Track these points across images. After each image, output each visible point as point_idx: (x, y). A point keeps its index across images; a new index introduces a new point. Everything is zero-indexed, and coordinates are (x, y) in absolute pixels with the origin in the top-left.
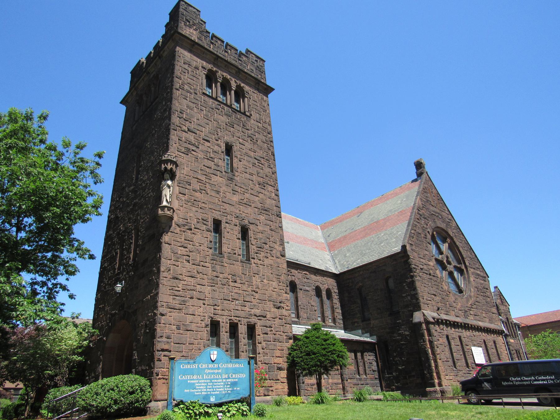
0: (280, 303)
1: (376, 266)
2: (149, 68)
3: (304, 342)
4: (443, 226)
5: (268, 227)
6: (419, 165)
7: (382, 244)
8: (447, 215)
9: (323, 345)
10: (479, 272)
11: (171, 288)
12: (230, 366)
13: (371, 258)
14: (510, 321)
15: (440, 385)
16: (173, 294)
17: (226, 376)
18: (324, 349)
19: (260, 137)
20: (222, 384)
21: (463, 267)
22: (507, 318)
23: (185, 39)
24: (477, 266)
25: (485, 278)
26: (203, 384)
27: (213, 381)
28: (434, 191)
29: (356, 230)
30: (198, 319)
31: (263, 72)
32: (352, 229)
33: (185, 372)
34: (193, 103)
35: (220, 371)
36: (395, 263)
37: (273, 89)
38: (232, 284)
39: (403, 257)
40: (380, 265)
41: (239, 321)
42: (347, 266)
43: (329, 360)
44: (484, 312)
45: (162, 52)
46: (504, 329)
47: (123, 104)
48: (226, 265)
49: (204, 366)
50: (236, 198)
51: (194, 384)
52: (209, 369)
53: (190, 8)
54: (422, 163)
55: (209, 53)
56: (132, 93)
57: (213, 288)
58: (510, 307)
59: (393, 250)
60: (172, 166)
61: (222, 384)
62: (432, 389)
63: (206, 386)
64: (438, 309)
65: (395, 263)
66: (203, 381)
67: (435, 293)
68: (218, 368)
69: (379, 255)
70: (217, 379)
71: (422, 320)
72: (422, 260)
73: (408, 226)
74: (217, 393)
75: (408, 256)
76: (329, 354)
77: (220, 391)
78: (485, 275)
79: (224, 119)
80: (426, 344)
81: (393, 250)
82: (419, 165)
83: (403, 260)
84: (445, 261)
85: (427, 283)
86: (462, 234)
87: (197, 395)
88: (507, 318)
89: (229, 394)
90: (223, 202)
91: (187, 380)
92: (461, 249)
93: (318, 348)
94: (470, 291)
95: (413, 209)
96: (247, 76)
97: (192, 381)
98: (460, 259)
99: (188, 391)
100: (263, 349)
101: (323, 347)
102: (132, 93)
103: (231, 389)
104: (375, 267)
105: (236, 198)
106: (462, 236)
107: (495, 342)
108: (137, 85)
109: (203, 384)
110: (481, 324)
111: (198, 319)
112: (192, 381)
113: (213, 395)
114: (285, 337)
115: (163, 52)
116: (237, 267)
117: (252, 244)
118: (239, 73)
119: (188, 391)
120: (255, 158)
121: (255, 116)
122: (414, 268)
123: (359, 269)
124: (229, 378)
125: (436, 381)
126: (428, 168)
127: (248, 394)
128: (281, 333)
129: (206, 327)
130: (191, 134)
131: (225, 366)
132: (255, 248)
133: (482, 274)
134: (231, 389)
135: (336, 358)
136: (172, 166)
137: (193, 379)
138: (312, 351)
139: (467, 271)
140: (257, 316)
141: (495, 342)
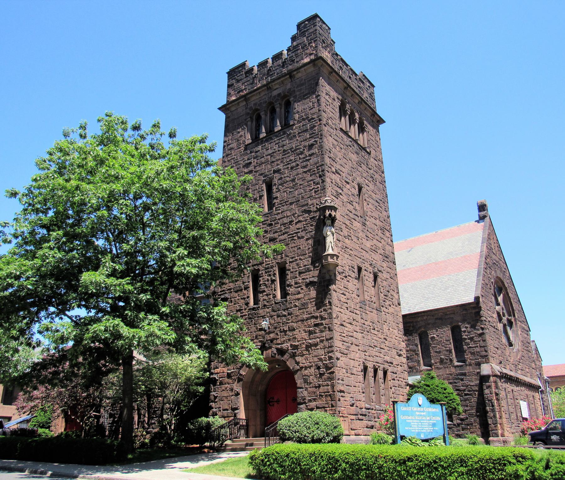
0: (400, 350)
1: (443, 313)
2: (273, 84)
3: (425, 389)
4: (501, 276)
5: (389, 274)
6: (482, 207)
7: (448, 291)
8: (502, 264)
9: (444, 393)
10: (524, 326)
11: (340, 334)
12: (430, 410)
13: (437, 303)
14: (542, 376)
15: (503, 435)
16: (342, 340)
17: (428, 418)
18: (446, 397)
19: (377, 176)
20: (427, 424)
21: (513, 320)
22: (540, 374)
23: (327, 66)
24: (523, 319)
25: (528, 331)
26: (415, 424)
27: (421, 421)
28: (495, 237)
29: (410, 269)
30: (357, 364)
31: (374, 100)
32: (404, 266)
33: (405, 413)
34: (336, 140)
35: (425, 413)
36: (464, 312)
37: (384, 122)
38: (372, 331)
39: (474, 308)
40: (448, 313)
41: (379, 367)
42: (408, 309)
43: (451, 407)
44: (527, 367)
45: (295, 73)
46: (541, 386)
47: (222, 111)
48: (368, 312)
49: (415, 409)
50: (368, 244)
51: (410, 423)
52: (418, 411)
53: (324, 26)
54: (485, 205)
55: (342, 81)
56: (238, 103)
57: (363, 335)
58: (542, 362)
59: (463, 299)
60: (330, 211)
61: (427, 424)
62: (495, 439)
63: (418, 425)
64: (501, 363)
65: (464, 312)
66: (415, 421)
67: (498, 346)
68: (423, 411)
69: (447, 302)
70: (423, 420)
71: (490, 373)
72: (489, 313)
73: (478, 276)
74: (424, 431)
75: (481, 307)
76: (451, 402)
77: (427, 430)
78: (528, 329)
79: (354, 157)
80: (493, 396)
81: (463, 299)
82: (482, 207)
83: (474, 311)
84: (501, 314)
85: (493, 336)
86: (513, 284)
87: (413, 432)
88: (540, 374)
89: (432, 432)
90: (362, 248)
91: (406, 419)
92: (512, 300)
93: (441, 395)
94: (517, 345)
95: (480, 257)
96: (367, 106)
97: (409, 421)
98: (511, 312)
99: (407, 428)
100: (393, 394)
101: (445, 395)
102: (238, 103)
103: (432, 429)
104: (442, 314)
105: (368, 244)
106: (512, 286)
107: (533, 396)
108: (249, 96)
109: (415, 424)
110: (528, 379)
111: (357, 364)
112: (409, 421)
113: (422, 432)
114: (404, 384)
115: (297, 73)
116: (374, 315)
117: (381, 292)
118: (361, 103)
119: (407, 428)
120: (376, 201)
121: (373, 152)
122: (485, 321)
123: (423, 314)
124: (430, 420)
125: (500, 432)
126: (491, 211)
127: (443, 433)
128: (402, 379)
129: (362, 371)
130: (338, 175)
131: (427, 410)
132: (383, 296)
133: (526, 328)
134: (432, 429)
135: (456, 406)
136: (330, 211)
137: (409, 419)
138: (435, 398)
139: (516, 324)
140: (388, 363)
141: (533, 396)
